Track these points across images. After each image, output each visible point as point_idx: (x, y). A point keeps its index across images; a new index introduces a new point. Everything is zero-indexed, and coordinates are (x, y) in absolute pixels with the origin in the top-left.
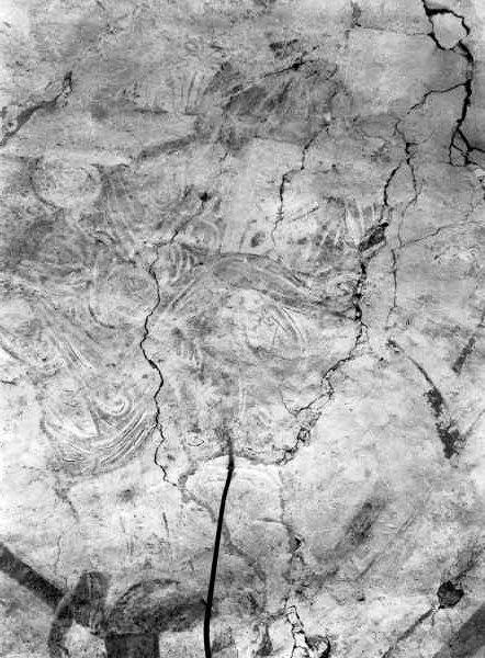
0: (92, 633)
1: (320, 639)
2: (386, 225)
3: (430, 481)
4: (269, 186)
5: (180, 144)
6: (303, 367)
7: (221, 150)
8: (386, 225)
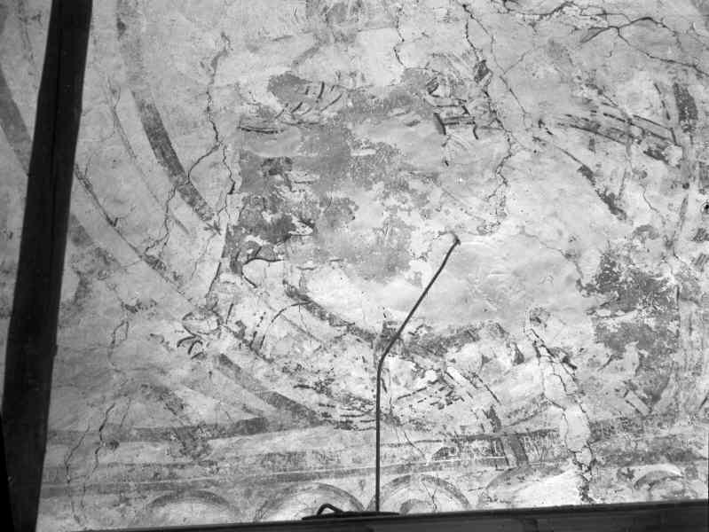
0: (330, 416)
1: (558, 350)
2: (484, 61)
3: (607, 232)
4: (387, 58)
5: (313, 51)
6: (479, 168)
7: (341, 45)
8: (484, 61)
